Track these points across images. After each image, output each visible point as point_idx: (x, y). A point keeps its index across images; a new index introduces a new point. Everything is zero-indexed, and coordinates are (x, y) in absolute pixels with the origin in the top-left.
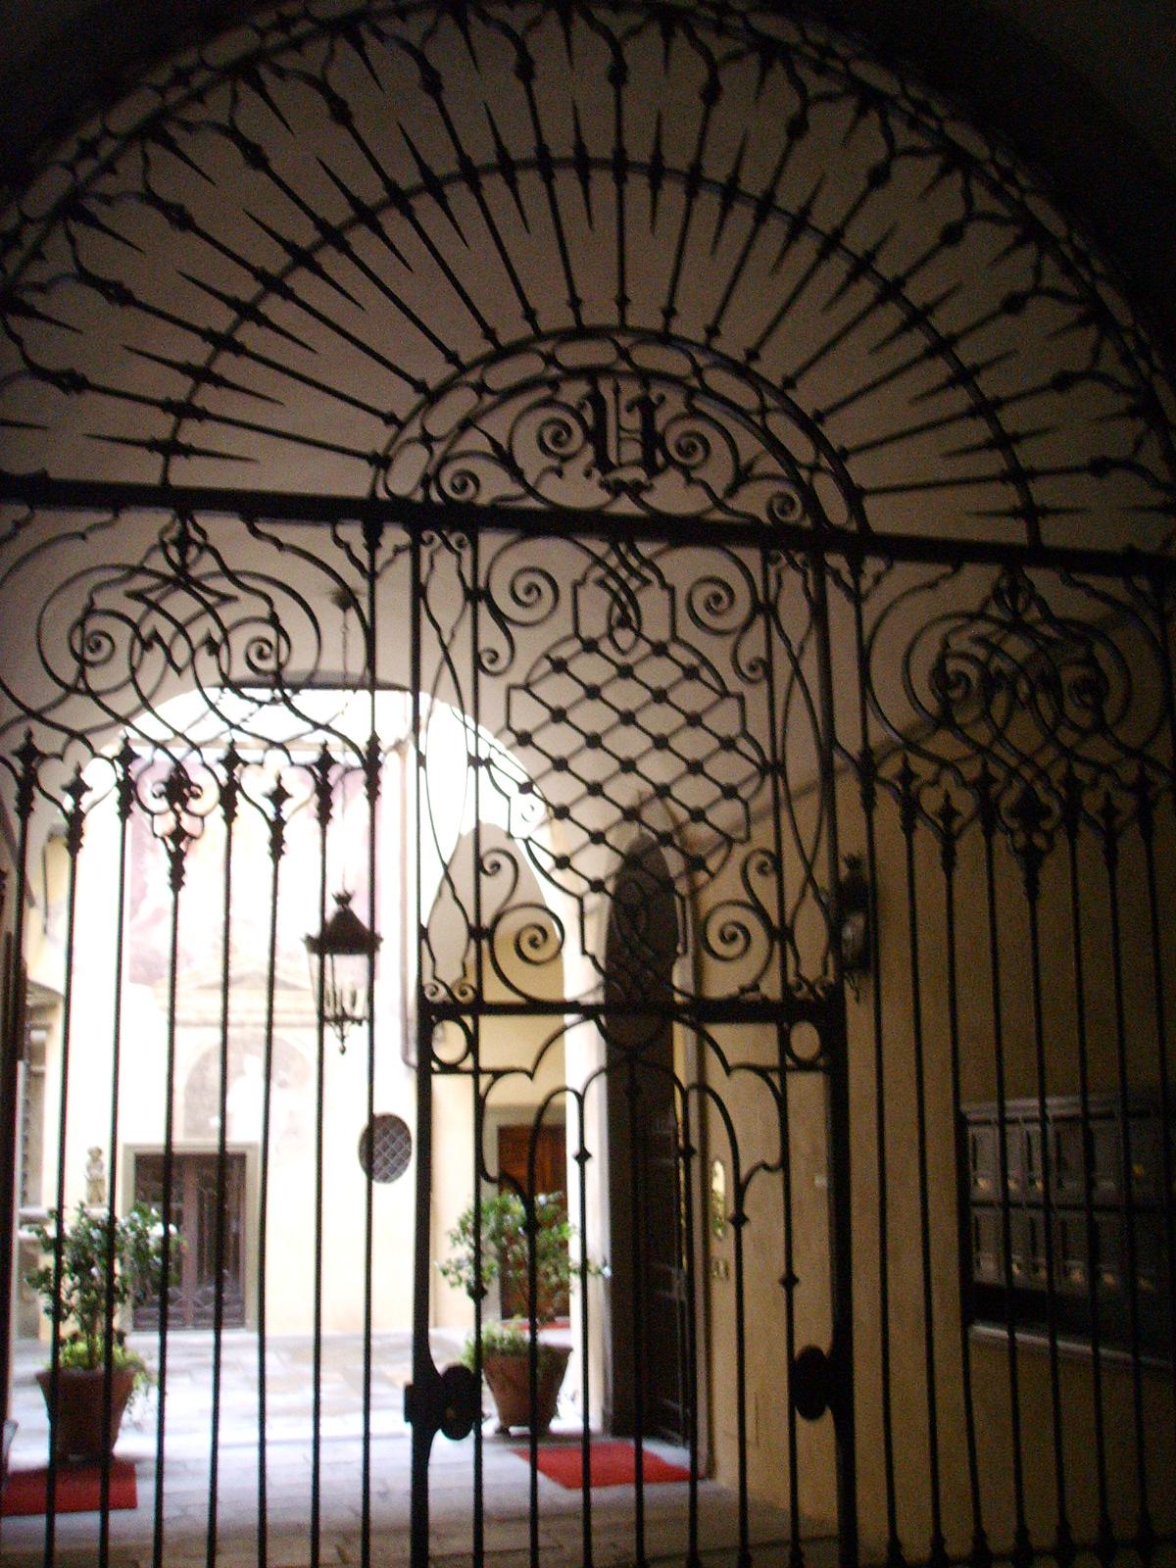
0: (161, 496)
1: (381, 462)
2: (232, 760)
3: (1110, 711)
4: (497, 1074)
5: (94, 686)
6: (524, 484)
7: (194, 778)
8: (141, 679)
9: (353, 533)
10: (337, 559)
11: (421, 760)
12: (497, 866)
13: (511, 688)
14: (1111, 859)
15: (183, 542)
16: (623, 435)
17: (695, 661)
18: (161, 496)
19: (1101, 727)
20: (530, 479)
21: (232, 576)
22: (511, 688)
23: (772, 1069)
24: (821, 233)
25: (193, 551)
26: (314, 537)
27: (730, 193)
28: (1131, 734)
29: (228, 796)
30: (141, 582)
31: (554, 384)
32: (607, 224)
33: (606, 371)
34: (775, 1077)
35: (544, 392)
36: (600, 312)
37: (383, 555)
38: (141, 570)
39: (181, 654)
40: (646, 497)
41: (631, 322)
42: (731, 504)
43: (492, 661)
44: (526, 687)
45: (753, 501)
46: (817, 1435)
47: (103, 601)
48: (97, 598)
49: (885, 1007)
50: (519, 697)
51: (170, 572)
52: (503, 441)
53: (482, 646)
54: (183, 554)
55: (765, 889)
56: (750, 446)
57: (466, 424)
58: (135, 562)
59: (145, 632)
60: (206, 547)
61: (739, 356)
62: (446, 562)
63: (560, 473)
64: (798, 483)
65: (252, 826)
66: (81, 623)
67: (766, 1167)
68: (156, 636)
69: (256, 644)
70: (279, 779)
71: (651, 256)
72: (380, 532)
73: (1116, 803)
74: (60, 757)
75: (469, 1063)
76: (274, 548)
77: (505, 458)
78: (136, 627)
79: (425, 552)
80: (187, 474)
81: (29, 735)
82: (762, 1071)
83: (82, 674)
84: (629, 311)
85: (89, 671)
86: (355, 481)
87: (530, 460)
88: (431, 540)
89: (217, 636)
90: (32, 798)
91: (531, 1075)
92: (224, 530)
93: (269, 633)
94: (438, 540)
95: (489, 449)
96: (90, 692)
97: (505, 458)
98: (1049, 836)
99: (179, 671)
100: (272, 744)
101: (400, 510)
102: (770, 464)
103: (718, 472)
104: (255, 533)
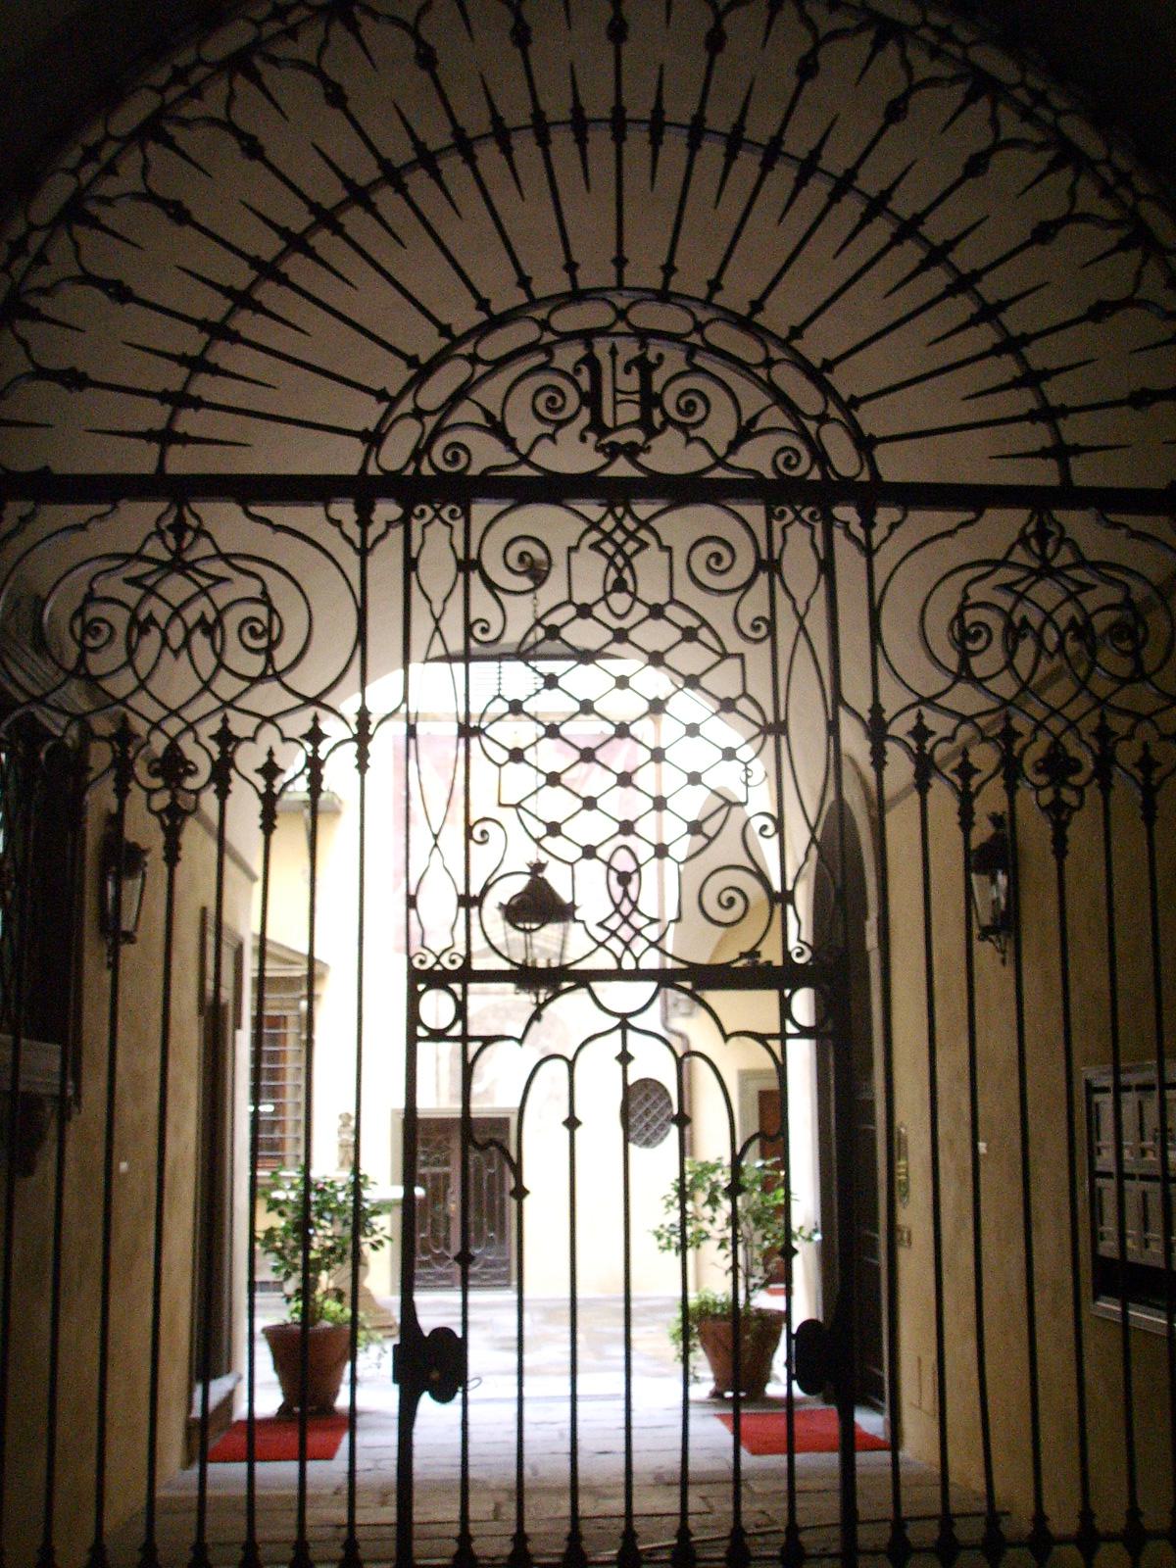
1: (373, 439)
4: (487, 1041)
6: (510, 443)
15: (179, 528)
16: (620, 397)
17: (695, 623)
20: (523, 449)
21: (226, 558)
23: (772, 1036)
25: (189, 536)
26: (308, 517)
29: (1105, 763)
35: (541, 358)
39: (176, 635)
43: (485, 631)
45: (757, 457)
47: (103, 588)
48: (971, 591)
54: (179, 538)
56: (753, 399)
57: (461, 394)
58: (132, 549)
60: (1062, 540)
63: (552, 437)
64: (804, 435)
66: (80, 612)
68: (151, 620)
70: (271, 753)
77: (497, 428)
78: (134, 613)
80: (182, 461)
82: (761, 1038)
86: (344, 458)
87: (524, 429)
89: (211, 617)
91: (521, 1041)
93: (261, 612)
94: (790, 516)
97: (497, 428)
99: (176, 653)
102: (776, 417)
103: (720, 428)
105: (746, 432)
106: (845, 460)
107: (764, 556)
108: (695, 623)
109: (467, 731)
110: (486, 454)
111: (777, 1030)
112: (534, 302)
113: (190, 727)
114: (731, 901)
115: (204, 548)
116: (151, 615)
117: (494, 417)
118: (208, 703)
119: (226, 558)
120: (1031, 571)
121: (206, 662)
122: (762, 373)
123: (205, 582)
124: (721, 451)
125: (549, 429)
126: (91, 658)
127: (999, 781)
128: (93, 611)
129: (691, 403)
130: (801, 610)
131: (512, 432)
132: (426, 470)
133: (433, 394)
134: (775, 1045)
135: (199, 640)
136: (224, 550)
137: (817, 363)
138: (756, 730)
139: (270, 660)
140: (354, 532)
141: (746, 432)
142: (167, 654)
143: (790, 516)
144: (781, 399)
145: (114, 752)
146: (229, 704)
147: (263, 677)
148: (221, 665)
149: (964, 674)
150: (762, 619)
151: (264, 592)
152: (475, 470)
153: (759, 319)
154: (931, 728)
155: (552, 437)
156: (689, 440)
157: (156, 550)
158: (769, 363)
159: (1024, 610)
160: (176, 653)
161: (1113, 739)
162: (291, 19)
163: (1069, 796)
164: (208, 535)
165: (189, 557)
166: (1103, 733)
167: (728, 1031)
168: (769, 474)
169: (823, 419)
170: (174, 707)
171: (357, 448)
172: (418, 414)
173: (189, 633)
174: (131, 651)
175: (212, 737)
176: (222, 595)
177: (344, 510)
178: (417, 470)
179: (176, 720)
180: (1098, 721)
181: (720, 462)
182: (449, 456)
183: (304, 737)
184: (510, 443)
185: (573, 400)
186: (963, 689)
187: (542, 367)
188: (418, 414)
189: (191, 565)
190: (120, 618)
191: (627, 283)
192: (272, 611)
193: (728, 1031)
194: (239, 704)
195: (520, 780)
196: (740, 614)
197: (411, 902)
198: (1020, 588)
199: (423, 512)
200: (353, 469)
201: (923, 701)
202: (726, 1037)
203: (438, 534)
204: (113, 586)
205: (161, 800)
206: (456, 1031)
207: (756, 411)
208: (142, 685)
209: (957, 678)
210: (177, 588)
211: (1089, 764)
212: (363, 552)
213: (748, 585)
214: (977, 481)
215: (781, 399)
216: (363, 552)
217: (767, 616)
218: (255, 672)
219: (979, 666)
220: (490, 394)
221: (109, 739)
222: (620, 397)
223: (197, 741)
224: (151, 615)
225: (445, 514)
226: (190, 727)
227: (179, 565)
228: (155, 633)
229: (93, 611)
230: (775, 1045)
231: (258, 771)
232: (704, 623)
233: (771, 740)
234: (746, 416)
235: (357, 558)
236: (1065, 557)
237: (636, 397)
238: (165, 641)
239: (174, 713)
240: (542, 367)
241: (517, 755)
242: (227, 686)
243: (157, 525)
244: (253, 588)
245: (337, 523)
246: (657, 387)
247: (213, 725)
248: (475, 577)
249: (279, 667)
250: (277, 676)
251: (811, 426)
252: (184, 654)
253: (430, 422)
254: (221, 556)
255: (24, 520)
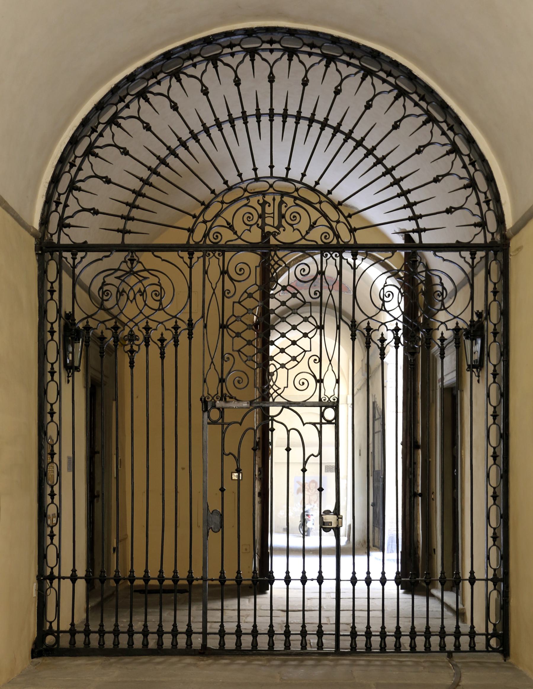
0: (121, 248)
1: (191, 231)
2: (147, 328)
3: (165, 302)
4: (229, 424)
6: (235, 233)
12: (228, 358)
13: (234, 303)
15: (132, 260)
16: (272, 215)
17: (296, 292)
18: (121, 248)
19: (161, 308)
20: (239, 234)
21: (148, 270)
22: (234, 303)
23: (318, 423)
24: (226, 121)
25: (135, 262)
27: (337, 130)
28: (172, 309)
30: (119, 273)
31: (248, 198)
33: (288, 194)
34: (319, 426)
35: (245, 202)
36: (294, 174)
37: (194, 260)
38: (119, 269)
39: (131, 296)
40: (278, 237)
43: (228, 293)
44: (239, 302)
45: (315, 236)
47: (108, 280)
48: (106, 279)
51: (128, 270)
52: (230, 221)
54: (132, 264)
55: (315, 368)
56: (315, 215)
57: (217, 216)
60: (139, 262)
61: (312, 184)
62: (214, 261)
63: (249, 230)
64: (331, 228)
65: (154, 349)
66: (101, 288)
67: (313, 455)
68: (123, 291)
69: (154, 293)
70: (162, 334)
71: (261, 148)
77: (231, 227)
80: (129, 239)
82: (314, 424)
83: (383, 305)
85: (386, 304)
86: (181, 238)
87: (239, 226)
89: (142, 290)
92: (146, 258)
93: (158, 288)
95: (226, 225)
96: (385, 310)
97: (231, 227)
99: (131, 301)
100: (160, 323)
101: (197, 247)
103: (304, 226)
105: (312, 226)
106: (345, 236)
107: (320, 269)
108: (296, 292)
109: (223, 326)
110: (227, 236)
111: (319, 421)
113: (136, 324)
115: (138, 267)
116: (123, 289)
117: (315, 224)
118: (141, 317)
119: (148, 270)
120: (127, 273)
121: (141, 303)
122: (317, 206)
123: (141, 278)
125: (248, 228)
126: (105, 303)
127: (453, 344)
128: (105, 288)
129: (294, 217)
130: (331, 288)
132: (208, 242)
133: (209, 214)
134: (318, 426)
135: (139, 298)
136: (147, 268)
137: (336, 203)
139: (161, 304)
140: (188, 261)
141: (312, 226)
143: (329, 255)
145: (394, 334)
146: (147, 317)
147: (159, 309)
148: (146, 304)
149: (101, 307)
150: (318, 291)
151: (159, 282)
152: (223, 242)
153: (318, 187)
154: (151, 326)
155: (249, 230)
157: (124, 267)
158: (320, 202)
159: (124, 286)
160: (131, 301)
161: (151, 330)
163: (135, 348)
164: (140, 262)
166: (147, 328)
168: (320, 243)
169: (338, 222)
170: (131, 318)
171: (187, 233)
173: (135, 295)
174: (118, 301)
175: (143, 328)
177: (185, 255)
179: (132, 323)
180: (367, 325)
181: (303, 238)
182: (215, 236)
183: (112, 328)
184: (235, 233)
185: (256, 217)
186: (101, 312)
187: (246, 205)
188: (205, 222)
189: (136, 272)
190: (114, 290)
192: (161, 288)
194: (150, 318)
195: (239, 343)
196: (112, 286)
197: (205, 381)
198: (122, 278)
199: (327, 255)
200: (184, 242)
201: (89, 316)
202: (304, 424)
205: (128, 348)
206: (323, 421)
207: (316, 219)
209: (100, 308)
210: (132, 280)
211: (141, 338)
212: (191, 267)
213: (314, 279)
214: (445, 243)
218: (156, 307)
219: (388, 306)
220: (228, 215)
221: (392, 331)
222: (272, 215)
223: (139, 330)
224: (123, 289)
225: (334, 255)
226: (136, 324)
227: (131, 272)
228: (125, 296)
229: (105, 288)
231: (158, 340)
232: (298, 292)
233: (319, 331)
236: (138, 267)
237: (266, 215)
239: (131, 320)
240: (246, 205)
241: (238, 335)
243: (125, 259)
244: (156, 281)
245: (182, 258)
246: (283, 212)
249: (446, 307)
250: (445, 309)
251: (334, 224)
252: (134, 301)
253: (209, 224)
254: (145, 270)
255: (82, 258)
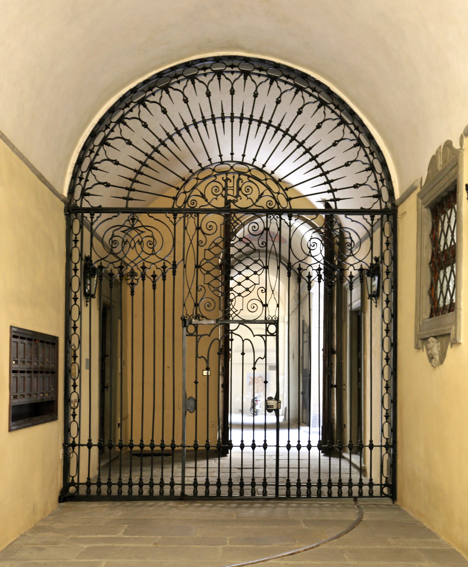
0: (126, 210)
1: (175, 199)
2: (144, 268)
3: (156, 249)
4: (201, 336)
5: (313, 255)
6: (206, 200)
7: (136, 272)
8: (124, 250)
9: (368, 217)
10: (364, 222)
11: (185, 266)
13: (205, 250)
14: (154, 287)
15: (133, 219)
16: (232, 188)
17: (249, 242)
18: (126, 210)
19: (154, 253)
20: (209, 201)
25: (135, 221)
26: (161, 216)
29: (143, 276)
30: (124, 229)
31: (215, 176)
32: (260, 135)
33: (243, 173)
39: (133, 245)
40: (236, 204)
41: (234, 160)
42: (256, 204)
43: (201, 243)
45: (263, 203)
46: (190, 417)
47: (116, 233)
49: (308, 324)
50: (207, 251)
51: (130, 226)
53: (199, 240)
54: (133, 222)
55: (262, 296)
56: (262, 188)
57: (194, 188)
58: (122, 224)
59: (125, 240)
61: (261, 167)
63: (216, 199)
64: (274, 197)
65: (148, 282)
66: (111, 239)
67: (260, 358)
68: (127, 241)
70: (154, 272)
72: (374, 217)
73: (156, 273)
74: (150, 268)
75: (268, 334)
76: (110, 220)
77: (203, 196)
78: (123, 239)
79: (186, 218)
80: (131, 204)
81: (300, 265)
82: (261, 336)
83: (310, 252)
84: (223, 157)
86: (168, 203)
87: (209, 196)
88: (270, 216)
89: (140, 240)
90: (301, 279)
91: (209, 336)
93: (151, 239)
94: (272, 217)
95: (200, 195)
96: (311, 256)
97: (203, 196)
98: (137, 280)
99: (133, 248)
100: (153, 264)
101: (179, 210)
102: (267, 193)
103: (254, 196)
104: (346, 217)
106: (284, 204)
107: (265, 226)
108: (249, 242)
109: (198, 267)
110: (201, 202)
111: (265, 334)
112: (232, 161)
114: (254, 307)
118: (139, 259)
121: (139, 250)
122: (264, 182)
123: (139, 232)
124: (254, 201)
125: (215, 197)
128: (114, 239)
129: (248, 189)
130: (273, 240)
131: (207, 197)
132: (187, 207)
133: (188, 187)
134: (264, 337)
135: (138, 246)
138: (261, 267)
139: (153, 250)
140: (173, 220)
141: (260, 196)
142: (131, 248)
143: (272, 217)
144: (269, 189)
146: (144, 260)
151: (152, 235)
152: (197, 207)
156: (248, 198)
157: (127, 224)
158: (266, 179)
160: (133, 248)
162: (179, 78)
163: (135, 281)
165: (135, 226)
167: (255, 334)
168: (266, 208)
169: (278, 193)
170: (132, 260)
171: (172, 201)
172: (185, 192)
173: (135, 244)
176: (143, 235)
177: (171, 216)
178: (185, 206)
181: (254, 204)
184: (206, 200)
187: (214, 181)
188: (185, 192)
189: (136, 228)
190: (120, 240)
191: (213, 163)
192: (154, 239)
193: (255, 334)
195: (209, 278)
197: (184, 305)
202: (254, 336)
203: (191, 220)
204: (117, 233)
208: (125, 256)
210: (133, 233)
212: (175, 224)
215: (269, 189)
216: (175, 224)
217: (265, 241)
218: (150, 253)
220: (201, 187)
222: (232, 188)
226: (136, 265)
227: (133, 228)
228: (128, 245)
229: (114, 239)
230: (264, 337)
233: (265, 270)
234: (261, 192)
235: (173, 226)
238: (130, 246)
239: (132, 262)
240: (214, 181)
242: (144, 256)
243: (128, 218)
247: (140, 265)
248: (200, 231)
251: (276, 195)
252: (134, 248)
253: (188, 194)
254: (143, 226)
